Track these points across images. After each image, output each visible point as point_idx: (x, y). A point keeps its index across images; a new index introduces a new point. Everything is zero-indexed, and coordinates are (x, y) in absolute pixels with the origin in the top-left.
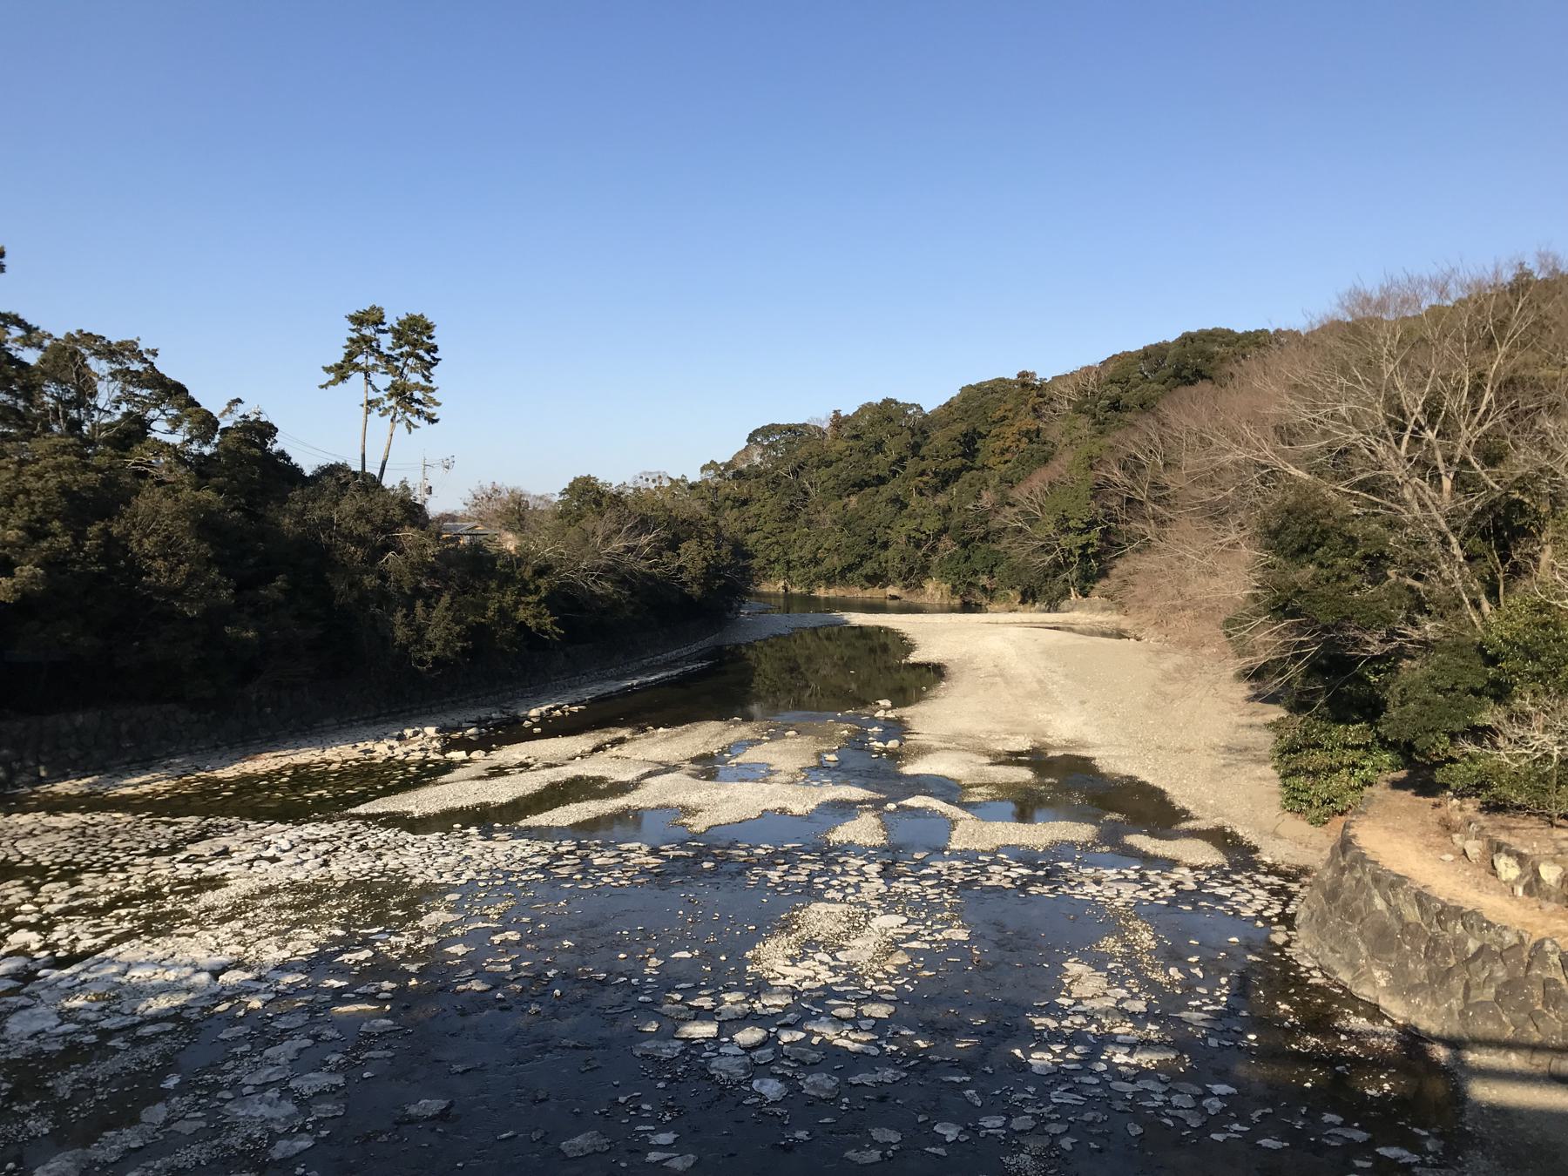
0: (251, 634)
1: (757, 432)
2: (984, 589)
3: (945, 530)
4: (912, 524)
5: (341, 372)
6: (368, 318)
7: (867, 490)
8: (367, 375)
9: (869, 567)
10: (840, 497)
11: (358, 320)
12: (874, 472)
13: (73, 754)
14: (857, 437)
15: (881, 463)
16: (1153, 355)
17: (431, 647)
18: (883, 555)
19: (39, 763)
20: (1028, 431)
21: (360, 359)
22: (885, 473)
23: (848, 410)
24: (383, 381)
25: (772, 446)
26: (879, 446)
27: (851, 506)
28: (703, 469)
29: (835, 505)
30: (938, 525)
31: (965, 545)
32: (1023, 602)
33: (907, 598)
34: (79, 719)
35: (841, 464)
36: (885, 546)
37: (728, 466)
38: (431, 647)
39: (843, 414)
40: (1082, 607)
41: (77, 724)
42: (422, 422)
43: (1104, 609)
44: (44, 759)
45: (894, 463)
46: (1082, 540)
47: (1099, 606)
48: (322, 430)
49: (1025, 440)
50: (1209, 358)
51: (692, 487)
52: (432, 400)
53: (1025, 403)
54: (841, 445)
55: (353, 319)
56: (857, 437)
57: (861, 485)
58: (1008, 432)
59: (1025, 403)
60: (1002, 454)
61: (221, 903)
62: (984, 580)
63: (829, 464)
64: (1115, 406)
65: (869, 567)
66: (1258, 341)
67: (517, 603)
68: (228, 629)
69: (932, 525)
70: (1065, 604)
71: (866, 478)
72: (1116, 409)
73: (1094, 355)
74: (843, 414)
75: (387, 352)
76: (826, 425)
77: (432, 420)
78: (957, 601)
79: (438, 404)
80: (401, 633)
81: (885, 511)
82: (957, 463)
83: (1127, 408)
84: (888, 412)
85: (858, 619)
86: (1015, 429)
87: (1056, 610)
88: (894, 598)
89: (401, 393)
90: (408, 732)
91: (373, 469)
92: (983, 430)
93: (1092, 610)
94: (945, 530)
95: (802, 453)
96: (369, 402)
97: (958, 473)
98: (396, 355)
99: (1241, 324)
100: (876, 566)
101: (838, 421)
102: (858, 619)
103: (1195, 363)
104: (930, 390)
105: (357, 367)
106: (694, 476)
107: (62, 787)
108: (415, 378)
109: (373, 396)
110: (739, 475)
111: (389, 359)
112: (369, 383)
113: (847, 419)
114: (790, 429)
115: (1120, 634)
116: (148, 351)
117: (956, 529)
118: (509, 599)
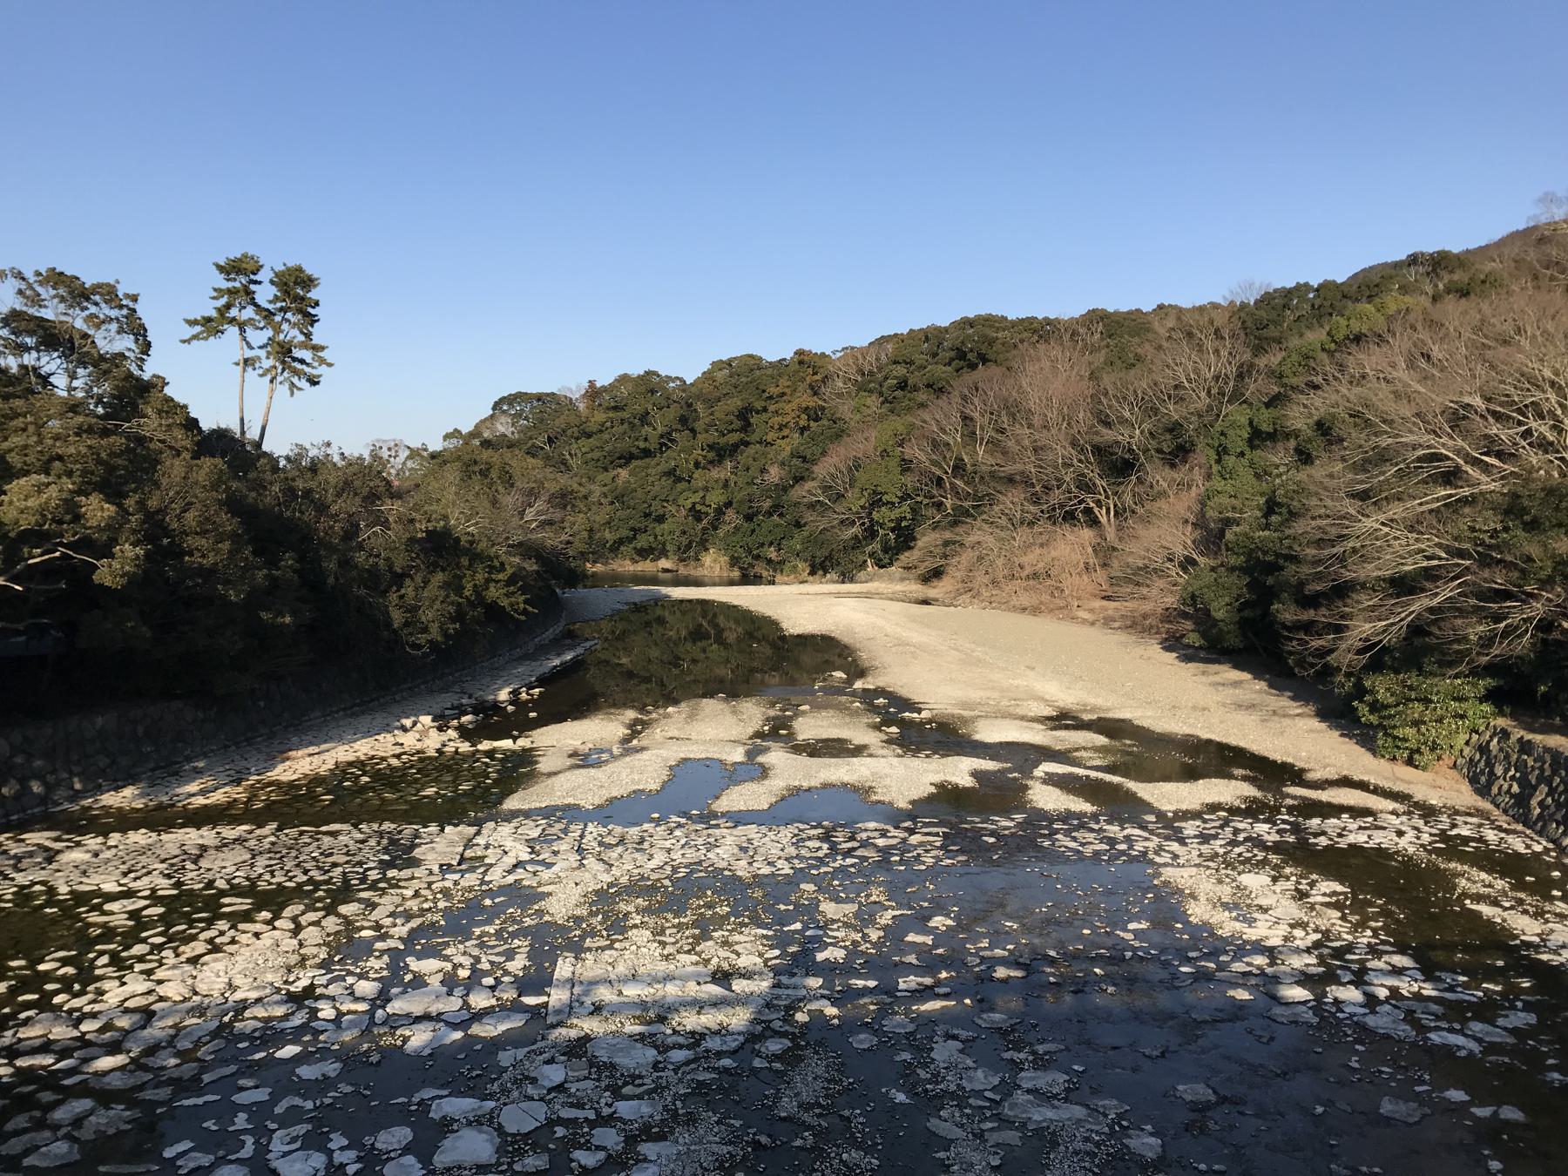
0: (288, 620)
1: (502, 400)
2: (770, 561)
3: (729, 504)
4: (696, 498)
5: (210, 326)
6: (240, 268)
7: (635, 463)
8: (242, 331)
9: (643, 541)
10: (606, 470)
11: (232, 268)
12: (642, 445)
13: (103, 761)
14: (615, 408)
15: (654, 432)
16: (932, 336)
17: (425, 630)
18: (659, 529)
19: (72, 774)
20: (807, 408)
21: (234, 312)
22: (653, 446)
23: (604, 380)
24: (259, 337)
25: (518, 415)
26: (644, 418)
27: (620, 482)
28: (447, 437)
29: (605, 477)
30: (723, 499)
31: (749, 518)
32: (812, 573)
33: (683, 571)
34: (99, 721)
35: (606, 436)
36: (661, 519)
37: (475, 434)
38: (425, 630)
39: (598, 385)
40: (881, 577)
41: (98, 727)
42: (303, 384)
43: (902, 579)
44: (76, 769)
45: (662, 436)
46: (895, 514)
47: (898, 575)
48: (211, 384)
49: (804, 416)
50: (991, 342)
51: (433, 456)
52: (322, 361)
53: (803, 380)
54: (600, 416)
55: (221, 268)
56: (615, 408)
57: (627, 458)
58: (788, 408)
59: (803, 380)
60: (780, 429)
61: (205, 926)
62: (772, 553)
63: (589, 436)
64: (903, 385)
65: (643, 541)
66: (1040, 331)
67: (488, 581)
68: (264, 615)
69: (716, 498)
70: (862, 575)
71: (634, 450)
72: (902, 389)
73: (862, 338)
74: (598, 385)
75: (265, 305)
76: (575, 396)
77: (313, 382)
78: (736, 574)
79: (330, 365)
80: (397, 617)
81: (661, 486)
82: (734, 438)
83: (916, 389)
84: (649, 384)
85: (678, 593)
86: (794, 405)
87: (852, 581)
88: (666, 571)
89: (284, 352)
90: (408, 722)
91: (253, 434)
92: (758, 405)
93: (891, 579)
94: (729, 504)
95: (560, 422)
96: (246, 361)
97: (734, 449)
98: (278, 309)
99: (1014, 311)
100: (651, 539)
101: (593, 392)
102: (678, 593)
103: (974, 348)
104: (686, 363)
105: (232, 321)
106: (436, 445)
107: (110, 799)
108: (295, 335)
109: (249, 354)
110: (486, 444)
111: (268, 315)
112: (245, 339)
113: (604, 389)
114: (539, 397)
115: (926, 602)
116: (127, 296)
117: (741, 502)
118: (480, 577)
